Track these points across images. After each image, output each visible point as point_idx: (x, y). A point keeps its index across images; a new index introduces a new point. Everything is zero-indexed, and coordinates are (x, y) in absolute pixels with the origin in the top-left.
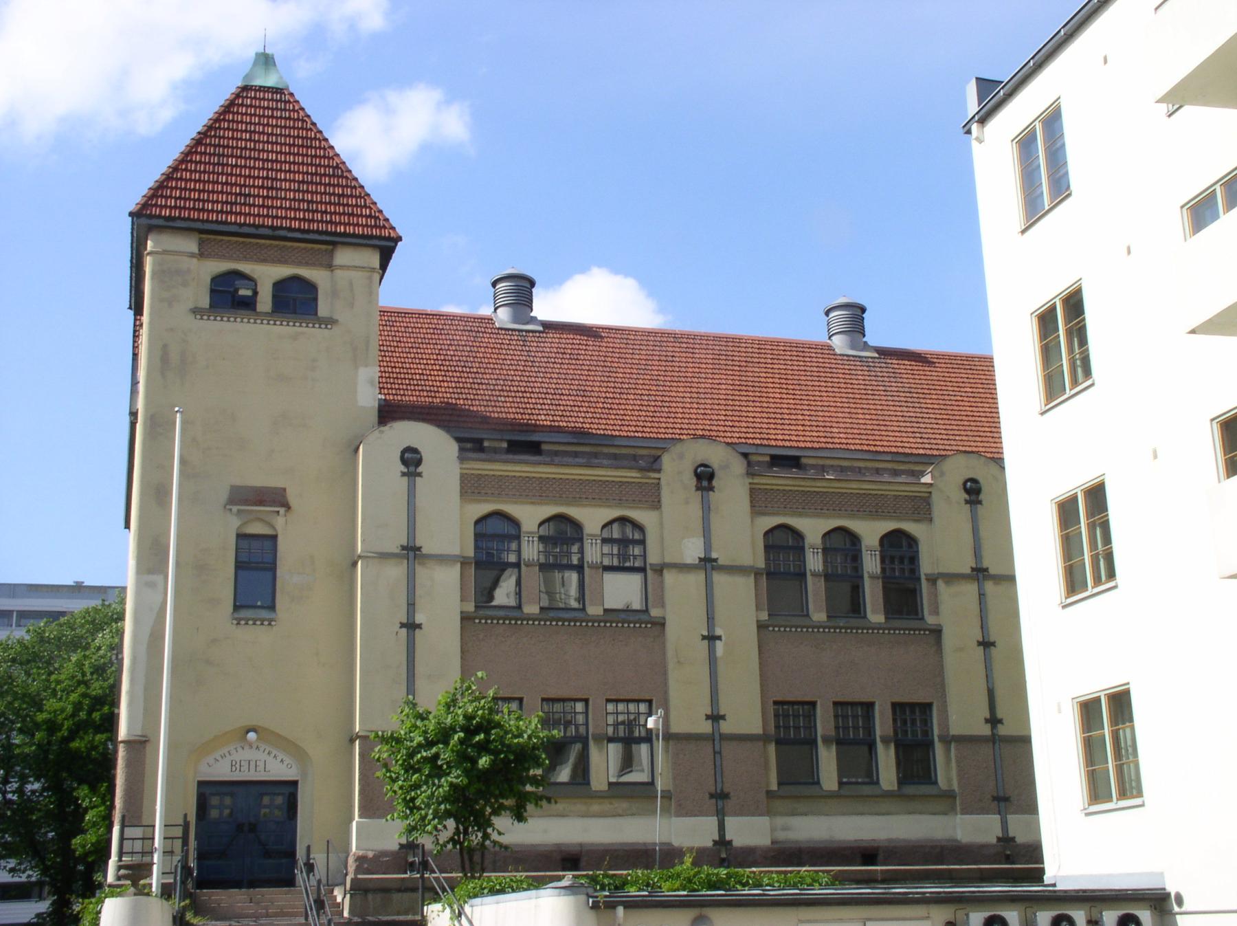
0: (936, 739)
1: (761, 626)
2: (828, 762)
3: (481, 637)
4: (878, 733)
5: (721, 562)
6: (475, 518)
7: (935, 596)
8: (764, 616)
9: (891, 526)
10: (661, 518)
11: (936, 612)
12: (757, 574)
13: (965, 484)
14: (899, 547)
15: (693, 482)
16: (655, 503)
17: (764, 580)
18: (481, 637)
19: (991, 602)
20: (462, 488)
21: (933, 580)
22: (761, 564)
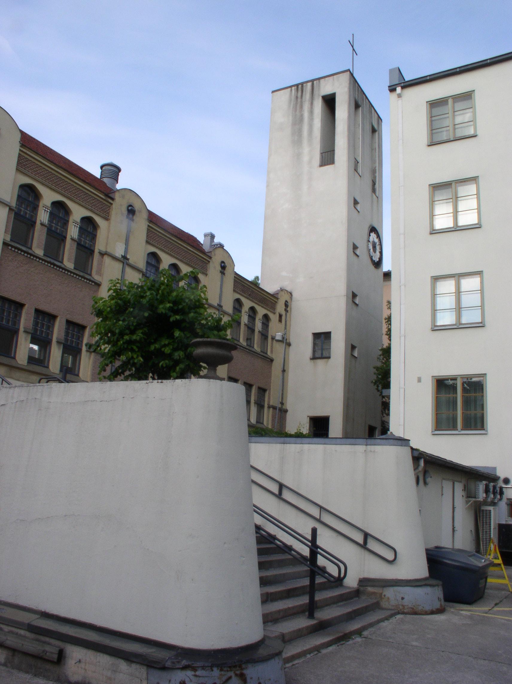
0: (22, 329)
1: (5, 244)
2: (56, 353)
3: (10, 258)
4: (85, 341)
5: (131, 261)
6: (83, 216)
7: (100, 264)
8: (8, 238)
9: (88, 214)
10: (109, 226)
11: (99, 273)
12: (11, 209)
13: (128, 208)
14: (89, 226)
15: (126, 212)
16: (107, 218)
17: (13, 216)
18: (10, 258)
19: (286, 350)
20: (18, 161)
21: (102, 254)
22: (14, 204)
